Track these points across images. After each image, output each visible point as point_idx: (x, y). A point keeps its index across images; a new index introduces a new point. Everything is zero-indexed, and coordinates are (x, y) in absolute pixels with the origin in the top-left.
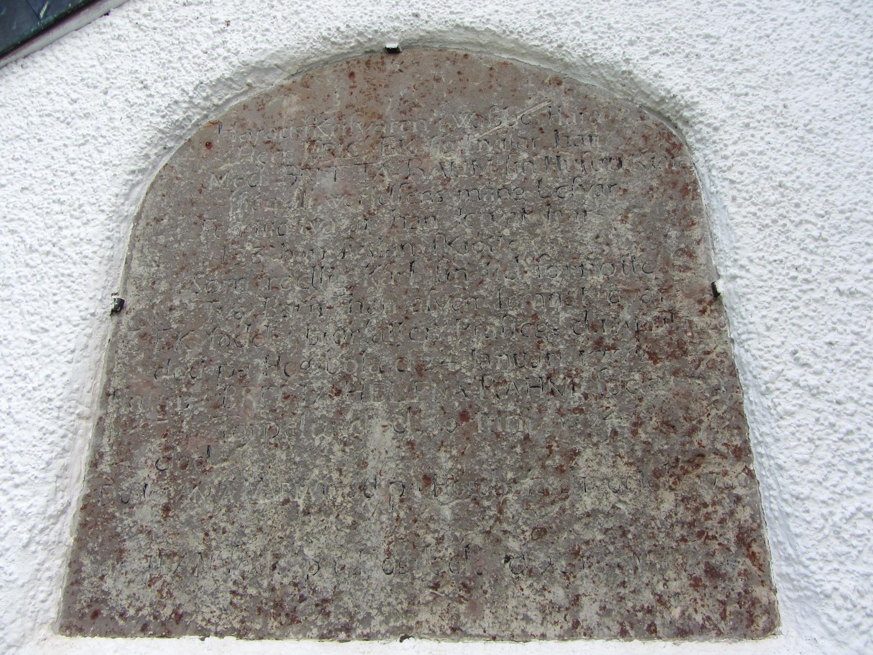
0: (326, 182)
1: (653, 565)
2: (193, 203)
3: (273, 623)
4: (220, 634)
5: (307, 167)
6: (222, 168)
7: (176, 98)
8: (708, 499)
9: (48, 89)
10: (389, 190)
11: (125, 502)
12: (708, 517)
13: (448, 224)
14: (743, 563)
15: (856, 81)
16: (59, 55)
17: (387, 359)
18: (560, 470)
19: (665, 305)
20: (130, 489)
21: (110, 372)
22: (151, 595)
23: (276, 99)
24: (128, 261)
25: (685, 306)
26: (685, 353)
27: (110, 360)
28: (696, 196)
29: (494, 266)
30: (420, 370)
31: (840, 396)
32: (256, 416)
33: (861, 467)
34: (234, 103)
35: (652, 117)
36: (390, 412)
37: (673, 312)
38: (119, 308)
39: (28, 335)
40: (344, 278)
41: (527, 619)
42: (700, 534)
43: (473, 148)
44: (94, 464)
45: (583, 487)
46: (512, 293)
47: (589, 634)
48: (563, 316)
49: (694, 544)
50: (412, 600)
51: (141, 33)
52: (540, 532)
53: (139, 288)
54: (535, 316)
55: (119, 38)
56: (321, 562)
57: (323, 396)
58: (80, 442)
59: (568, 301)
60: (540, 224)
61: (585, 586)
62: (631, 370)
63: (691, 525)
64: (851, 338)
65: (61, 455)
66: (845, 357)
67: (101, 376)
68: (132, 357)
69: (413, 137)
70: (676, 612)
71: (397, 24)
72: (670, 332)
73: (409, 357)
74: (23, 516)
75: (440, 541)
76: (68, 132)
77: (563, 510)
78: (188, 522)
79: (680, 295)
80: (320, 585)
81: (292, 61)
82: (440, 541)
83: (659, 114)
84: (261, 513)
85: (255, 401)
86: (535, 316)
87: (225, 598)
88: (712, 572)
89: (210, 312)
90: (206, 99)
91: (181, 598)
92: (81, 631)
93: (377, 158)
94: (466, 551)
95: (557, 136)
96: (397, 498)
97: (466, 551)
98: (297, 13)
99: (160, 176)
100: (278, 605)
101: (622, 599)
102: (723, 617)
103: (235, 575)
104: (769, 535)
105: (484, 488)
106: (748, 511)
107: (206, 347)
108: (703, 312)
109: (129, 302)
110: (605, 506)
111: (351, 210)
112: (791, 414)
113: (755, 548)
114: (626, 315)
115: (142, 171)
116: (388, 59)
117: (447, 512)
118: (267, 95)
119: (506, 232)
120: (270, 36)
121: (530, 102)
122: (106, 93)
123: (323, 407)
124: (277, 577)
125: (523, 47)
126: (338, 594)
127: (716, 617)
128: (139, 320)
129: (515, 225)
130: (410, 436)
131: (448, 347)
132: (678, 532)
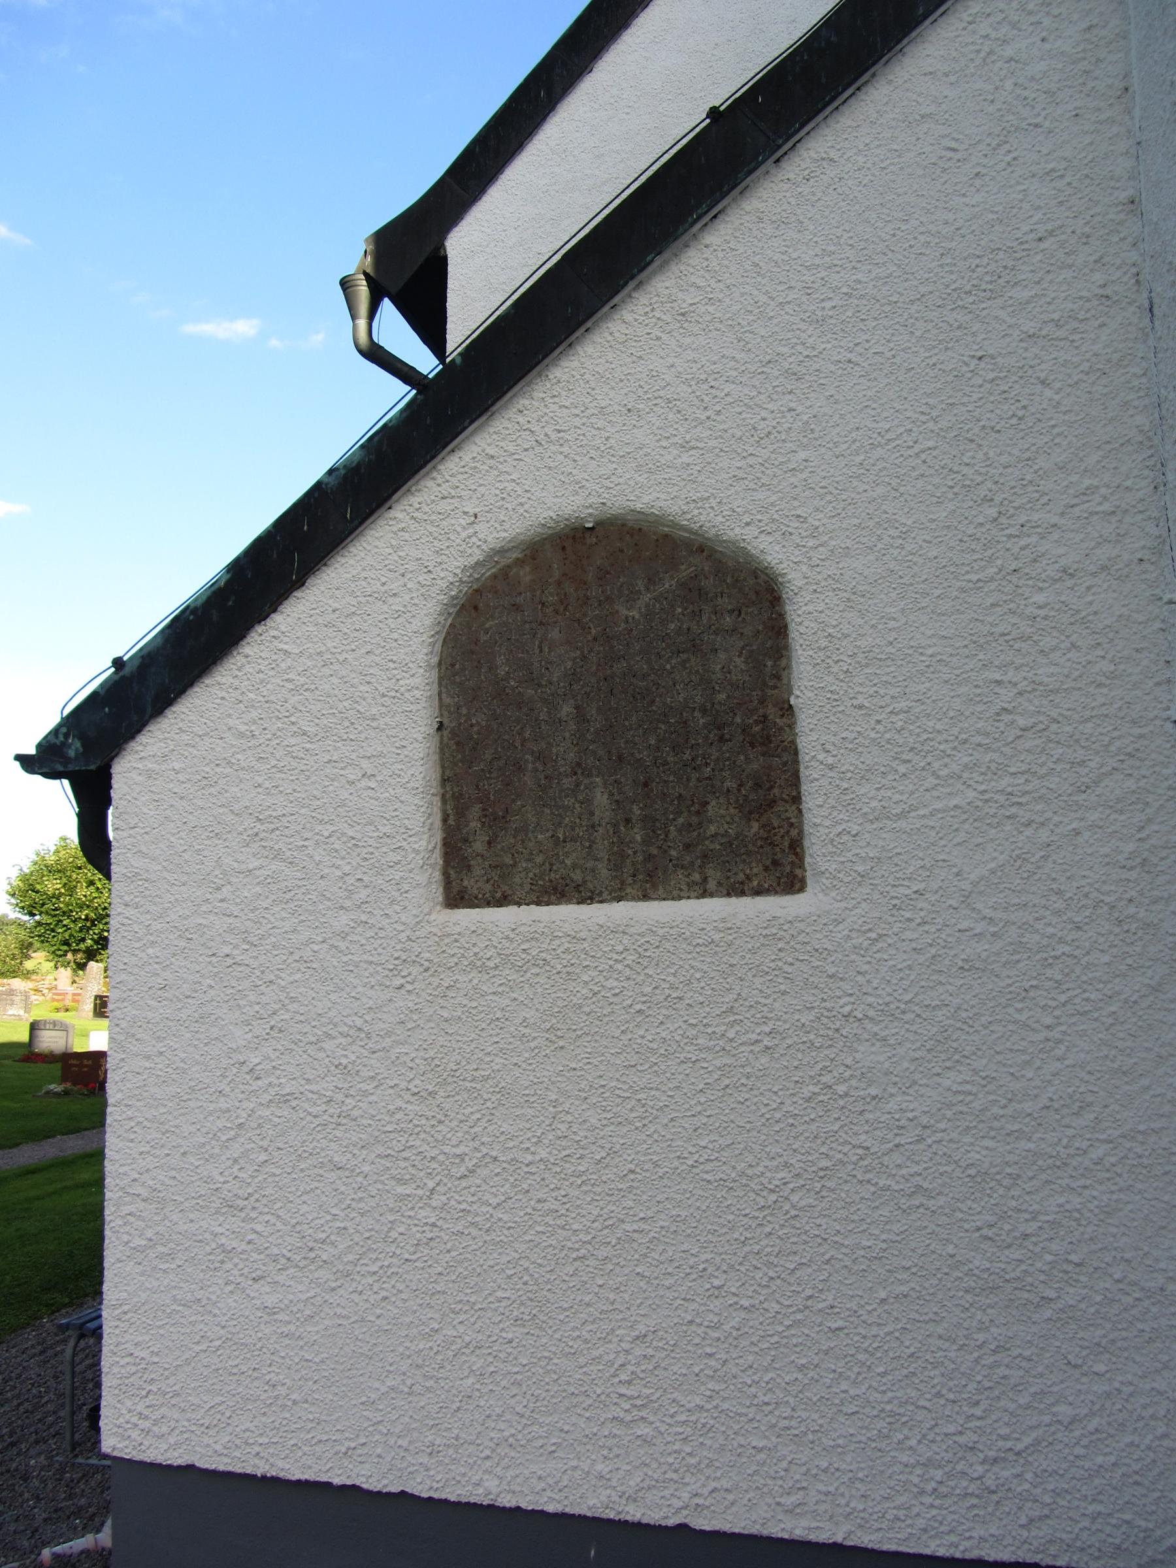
0: (555, 634)
1: (745, 861)
2: (472, 652)
3: (553, 898)
4: (528, 904)
5: (541, 623)
6: (487, 626)
7: (451, 580)
8: (776, 825)
9: (364, 574)
10: (595, 639)
11: (466, 840)
12: (775, 835)
13: (632, 663)
14: (792, 858)
15: (891, 551)
16: (365, 545)
17: (601, 753)
18: (698, 813)
19: (761, 712)
20: (468, 833)
21: (443, 767)
22: (489, 887)
23: (515, 570)
24: (440, 694)
25: (772, 711)
26: (770, 742)
27: (442, 759)
28: (786, 635)
29: (662, 690)
30: (620, 758)
31: (843, 769)
32: (531, 790)
33: (849, 808)
34: (488, 574)
35: (763, 576)
36: (605, 784)
37: (765, 716)
38: (441, 727)
39: (394, 750)
40: (572, 701)
41: (681, 890)
42: (770, 844)
43: (647, 605)
44: (445, 820)
45: (710, 821)
46: (672, 708)
47: (712, 895)
48: (702, 721)
49: (768, 849)
50: (623, 883)
51: (417, 525)
52: (687, 846)
53: (449, 712)
54: (685, 722)
55: (403, 530)
56: (575, 866)
57: (567, 776)
58: (435, 809)
59: (704, 711)
60: (688, 660)
61: (710, 872)
62: (739, 753)
63: (766, 839)
64: (855, 735)
65: (428, 818)
66: (851, 746)
67: (438, 769)
68: (454, 757)
69: (607, 598)
70: (755, 883)
71: (591, 511)
72: (763, 729)
73: (614, 751)
74: (417, 852)
75: (635, 853)
76: (385, 608)
77: (699, 834)
78: (502, 849)
79: (770, 706)
80: (575, 878)
81: (522, 542)
82: (635, 853)
83: (767, 574)
84: (540, 843)
85: (528, 779)
86: (685, 722)
87: (527, 887)
88: (775, 863)
89: (495, 726)
90: (471, 576)
91: (505, 888)
92: (796, 847)
93: (585, 615)
94: (649, 857)
95: (700, 595)
96: (611, 832)
97: (649, 857)
98: (521, 504)
99: (448, 633)
100: (555, 889)
101: (728, 878)
102: (779, 884)
103: (531, 875)
104: (806, 843)
105: (658, 825)
106: (796, 831)
107: (496, 749)
108: (782, 716)
109: (446, 721)
110: (722, 831)
111: (573, 655)
112: (817, 780)
113: (798, 850)
114: (738, 720)
115: (437, 633)
116: (587, 535)
117: (638, 838)
118: (508, 566)
119: (668, 667)
120: (507, 526)
121: (683, 567)
122: (403, 575)
123: (567, 782)
124: (553, 875)
125: (677, 524)
126: (585, 882)
127: (775, 884)
128: (452, 732)
129: (674, 661)
130: (616, 797)
131: (636, 744)
132: (759, 843)
